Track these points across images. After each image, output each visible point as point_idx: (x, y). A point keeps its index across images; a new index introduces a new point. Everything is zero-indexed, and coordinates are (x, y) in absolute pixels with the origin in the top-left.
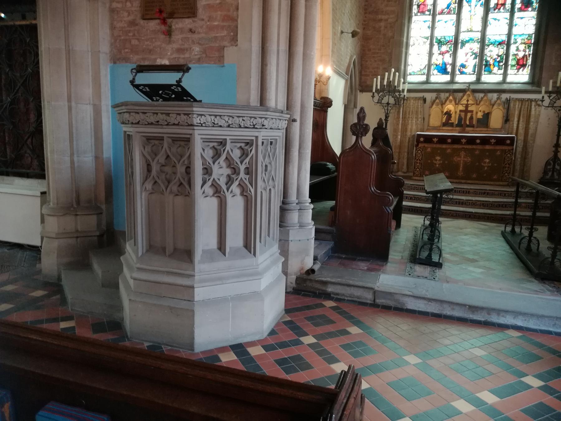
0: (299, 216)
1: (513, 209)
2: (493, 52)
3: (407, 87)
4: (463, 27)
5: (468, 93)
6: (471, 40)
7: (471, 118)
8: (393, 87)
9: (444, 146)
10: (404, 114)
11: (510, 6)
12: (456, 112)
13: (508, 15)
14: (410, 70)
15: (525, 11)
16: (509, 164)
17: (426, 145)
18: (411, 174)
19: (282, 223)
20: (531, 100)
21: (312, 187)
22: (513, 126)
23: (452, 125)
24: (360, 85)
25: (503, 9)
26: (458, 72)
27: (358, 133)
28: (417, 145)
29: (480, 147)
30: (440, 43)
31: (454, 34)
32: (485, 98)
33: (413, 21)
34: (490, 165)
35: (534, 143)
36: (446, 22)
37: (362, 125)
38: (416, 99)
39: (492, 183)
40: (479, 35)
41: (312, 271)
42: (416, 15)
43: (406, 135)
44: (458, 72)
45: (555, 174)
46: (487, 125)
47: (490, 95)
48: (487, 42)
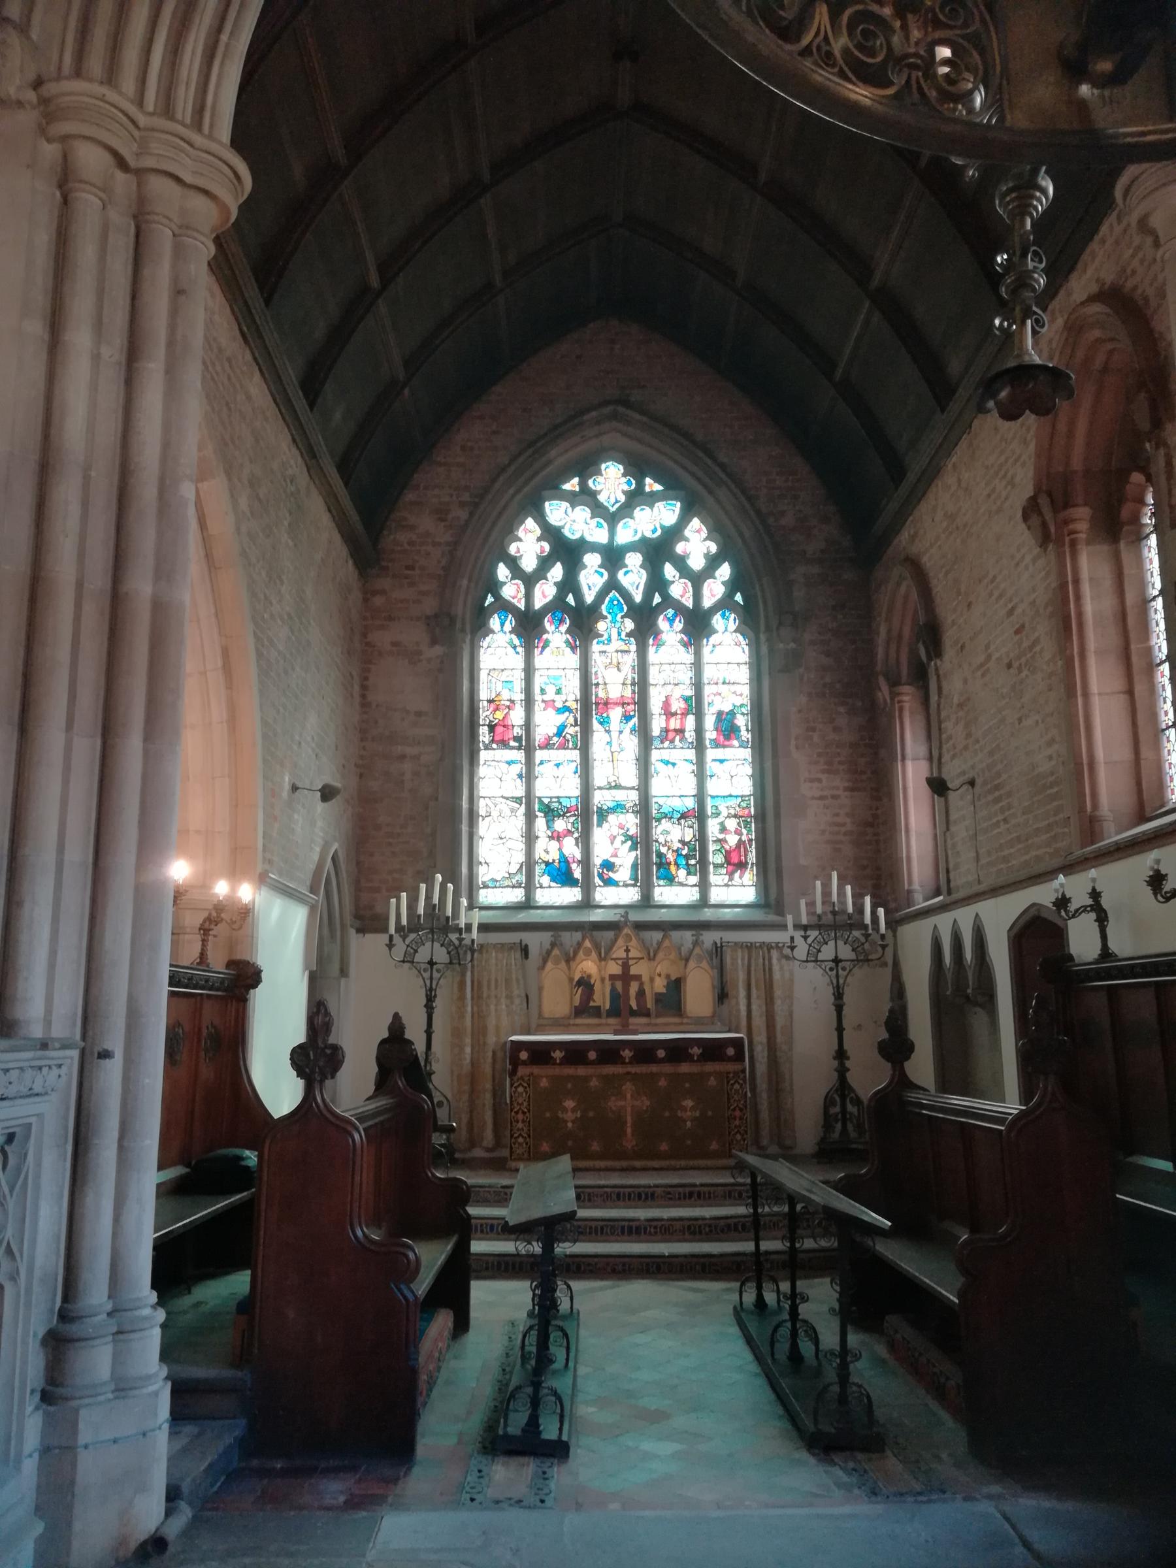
0: (116, 1357)
1: (752, 1235)
2: (671, 835)
3: (477, 917)
4: (600, 776)
5: (626, 931)
6: (619, 808)
7: (641, 994)
8: (443, 920)
9: (581, 1071)
10: (477, 986)
11: (693, 734)
12: (603, 980)
13: (691, 754)
14: (484, 874)
15: (724, 746)
16: (741, 1110)
17: (536, 1070)
18: (505, 1153)
19: (54, 1392)
20: (769, 947)
21: (160, 1247)
22: (738, 1011)
23: (597, 1012)
24: (357, 916)
25: (681, 740)
26: (597, 881)
27: (313, 1072)
28: (513, 1073)
29: (668, 1068)
30: (550, 813)
31: (578, 793)
32: (666, 943)
33: (482, 762)
34: (697, 1114)
35: (791, 1049)
36: (557, 765)
37: (323, 1050)
38: (502, 947)
39: (709, 1163)
40: (634, 796)
41: (157, 1543)
42: (487, 748)
43: (485, 1044)
44: (597, 881)
45: (850, 1127)
46: (680, 1009)
47: (675, 935)
48: (654, 812)
